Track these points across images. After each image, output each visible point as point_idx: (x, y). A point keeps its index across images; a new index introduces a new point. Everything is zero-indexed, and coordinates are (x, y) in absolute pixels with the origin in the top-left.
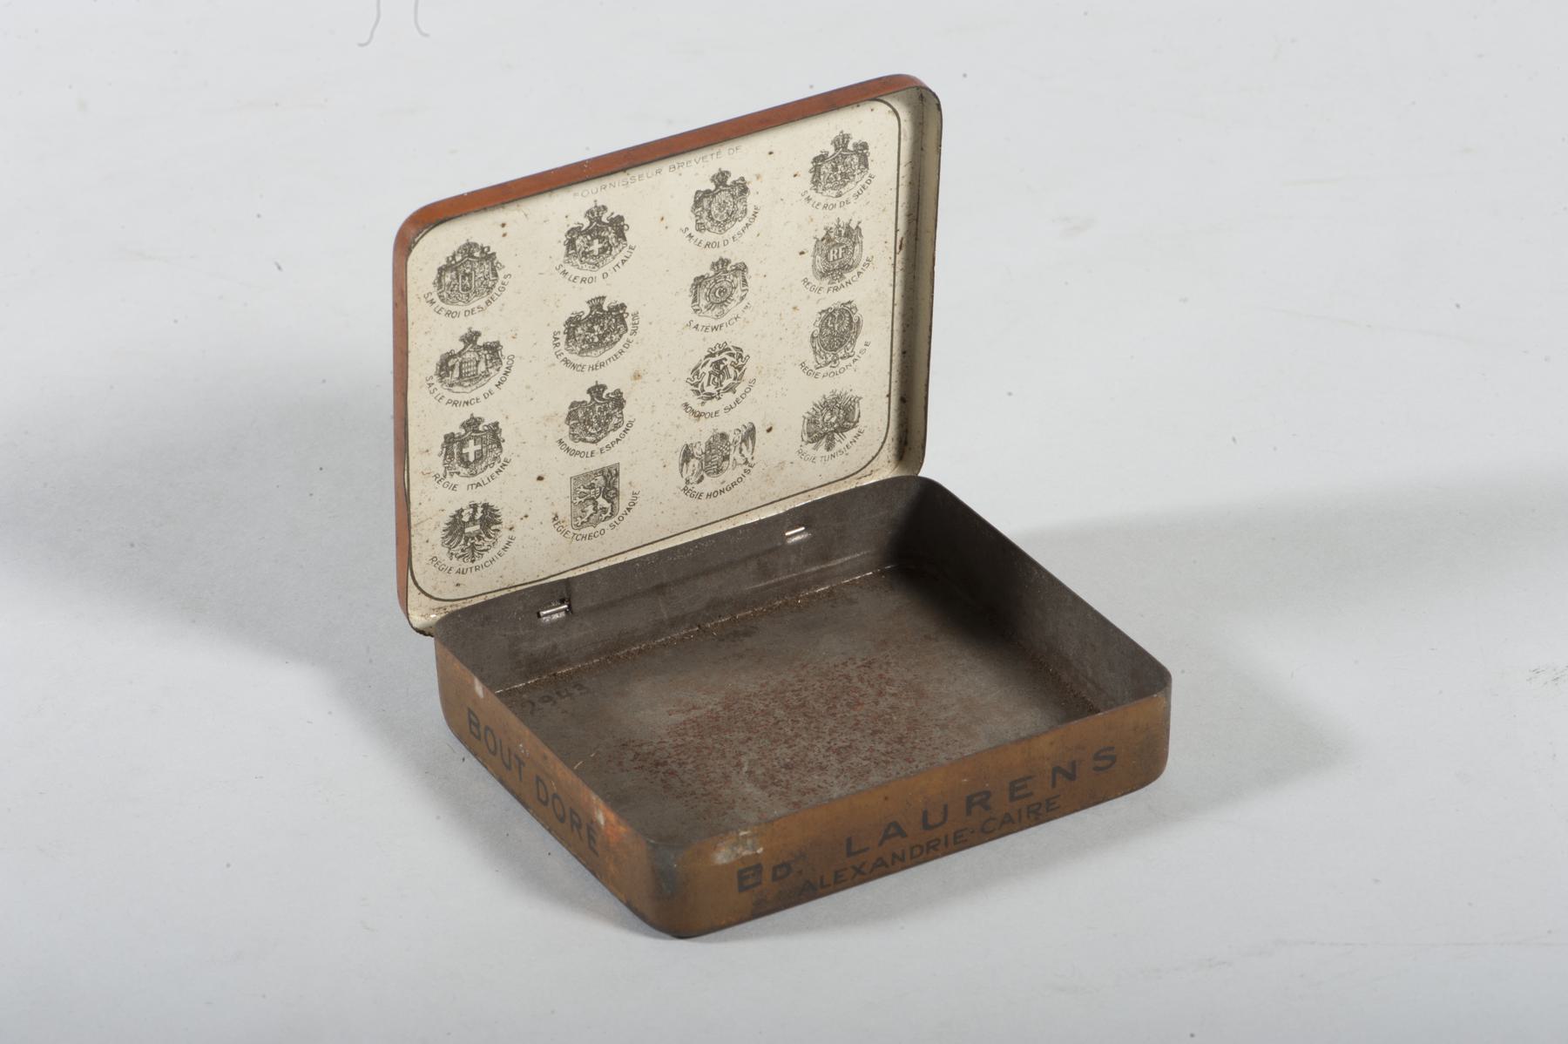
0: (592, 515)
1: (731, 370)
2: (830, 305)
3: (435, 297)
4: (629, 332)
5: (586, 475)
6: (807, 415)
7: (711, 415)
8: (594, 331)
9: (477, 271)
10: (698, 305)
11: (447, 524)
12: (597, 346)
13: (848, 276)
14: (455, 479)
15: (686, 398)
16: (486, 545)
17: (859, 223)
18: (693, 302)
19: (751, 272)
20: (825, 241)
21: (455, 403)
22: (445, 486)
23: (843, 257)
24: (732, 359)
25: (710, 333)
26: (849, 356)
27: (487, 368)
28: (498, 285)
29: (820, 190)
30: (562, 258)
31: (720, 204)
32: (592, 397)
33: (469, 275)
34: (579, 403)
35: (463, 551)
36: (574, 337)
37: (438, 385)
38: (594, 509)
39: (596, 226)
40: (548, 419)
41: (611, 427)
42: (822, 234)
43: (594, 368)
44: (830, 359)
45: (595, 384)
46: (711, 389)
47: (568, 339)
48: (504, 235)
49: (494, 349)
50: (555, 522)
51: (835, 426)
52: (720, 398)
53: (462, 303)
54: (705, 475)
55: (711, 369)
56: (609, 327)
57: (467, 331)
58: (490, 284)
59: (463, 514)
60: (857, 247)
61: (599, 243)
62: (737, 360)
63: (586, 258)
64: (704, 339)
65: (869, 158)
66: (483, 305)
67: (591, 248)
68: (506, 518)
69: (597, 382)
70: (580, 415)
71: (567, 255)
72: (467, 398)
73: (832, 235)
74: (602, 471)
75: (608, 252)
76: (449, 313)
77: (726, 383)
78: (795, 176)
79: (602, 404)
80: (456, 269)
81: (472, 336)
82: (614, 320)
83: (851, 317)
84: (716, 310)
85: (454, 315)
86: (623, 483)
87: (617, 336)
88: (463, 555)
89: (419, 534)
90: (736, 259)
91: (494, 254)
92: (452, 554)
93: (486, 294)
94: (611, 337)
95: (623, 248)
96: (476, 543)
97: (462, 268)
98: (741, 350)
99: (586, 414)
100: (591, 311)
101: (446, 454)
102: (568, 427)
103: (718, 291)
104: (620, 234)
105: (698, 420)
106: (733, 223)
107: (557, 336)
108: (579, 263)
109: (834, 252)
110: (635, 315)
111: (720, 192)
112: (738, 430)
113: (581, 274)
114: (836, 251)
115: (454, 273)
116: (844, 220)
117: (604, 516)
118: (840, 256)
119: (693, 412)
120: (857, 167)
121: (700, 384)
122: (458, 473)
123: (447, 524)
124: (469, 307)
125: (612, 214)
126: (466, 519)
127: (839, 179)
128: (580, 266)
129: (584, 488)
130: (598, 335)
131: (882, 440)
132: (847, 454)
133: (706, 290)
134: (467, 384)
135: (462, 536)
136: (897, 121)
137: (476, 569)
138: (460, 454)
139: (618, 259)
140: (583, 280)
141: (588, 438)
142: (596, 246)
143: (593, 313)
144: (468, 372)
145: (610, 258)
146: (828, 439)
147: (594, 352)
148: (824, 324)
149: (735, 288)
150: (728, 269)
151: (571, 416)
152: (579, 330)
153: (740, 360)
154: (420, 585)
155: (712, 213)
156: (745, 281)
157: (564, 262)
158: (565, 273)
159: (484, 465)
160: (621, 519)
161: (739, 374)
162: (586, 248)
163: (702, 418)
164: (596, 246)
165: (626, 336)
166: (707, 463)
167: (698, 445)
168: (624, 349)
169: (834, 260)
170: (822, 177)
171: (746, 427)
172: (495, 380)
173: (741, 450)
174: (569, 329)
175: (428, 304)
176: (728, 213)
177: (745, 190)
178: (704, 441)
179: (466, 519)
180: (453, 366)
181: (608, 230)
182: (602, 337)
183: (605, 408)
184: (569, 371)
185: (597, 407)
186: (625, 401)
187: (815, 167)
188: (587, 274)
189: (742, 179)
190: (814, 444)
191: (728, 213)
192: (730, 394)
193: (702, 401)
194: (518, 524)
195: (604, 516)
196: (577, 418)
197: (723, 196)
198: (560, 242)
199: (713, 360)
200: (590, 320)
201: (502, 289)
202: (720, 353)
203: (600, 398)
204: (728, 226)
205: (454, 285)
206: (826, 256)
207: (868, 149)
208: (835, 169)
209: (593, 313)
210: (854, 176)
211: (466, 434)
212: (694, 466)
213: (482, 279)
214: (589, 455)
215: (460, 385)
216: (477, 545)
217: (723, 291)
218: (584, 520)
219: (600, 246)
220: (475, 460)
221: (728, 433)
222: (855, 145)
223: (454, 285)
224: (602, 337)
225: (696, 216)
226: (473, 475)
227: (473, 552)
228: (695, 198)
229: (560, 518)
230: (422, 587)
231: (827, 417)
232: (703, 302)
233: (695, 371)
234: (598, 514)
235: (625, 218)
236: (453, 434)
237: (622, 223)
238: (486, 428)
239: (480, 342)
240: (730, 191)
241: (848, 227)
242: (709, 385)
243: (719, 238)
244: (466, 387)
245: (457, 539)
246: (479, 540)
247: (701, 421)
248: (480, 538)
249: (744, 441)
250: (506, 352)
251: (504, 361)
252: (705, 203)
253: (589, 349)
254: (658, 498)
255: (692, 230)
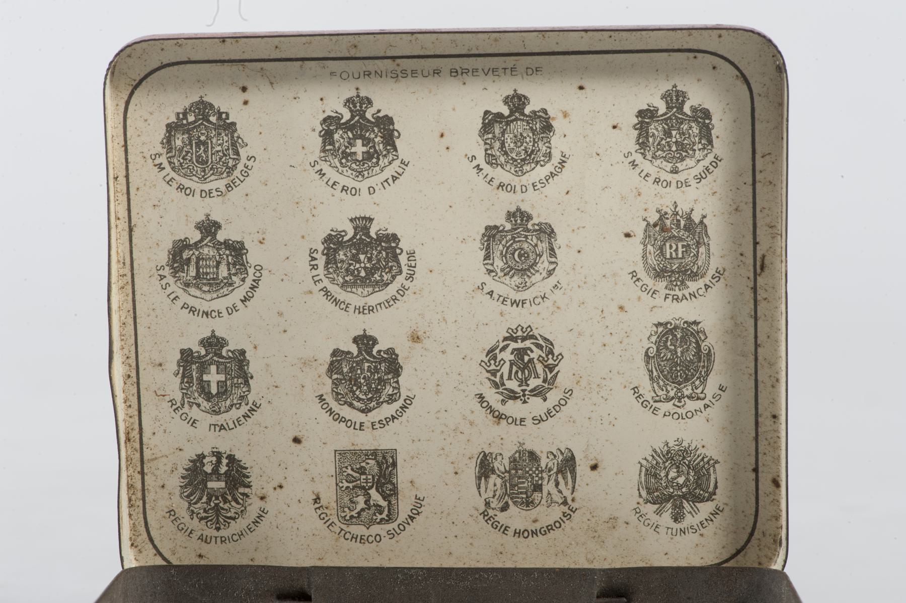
0: (363, 510)
1: (540, 368)
2: (669, 319)
3: (163, 160)
4: (404, 274)
5: (354, 453)
6: (644, 463)
7: (514, 421)
8: (359, 261)
9: (214, 140)
10: (492, 265)
11: (186, 470)
12: (364, 282)
13: (693, 286)
14: (195, 413)
15: (480, 387)
16: (233, 511)
17: (704, 217)
18: (485, 260)
19: (561, 240)
20: (658, 228)
21: (192, 310)
22: (183, 417)
23: (683, 257)
24: (540, 352)
25: (508, 308)
26: (698, 399)
27: (230, 274)
28: (240, 167)
29: (649, 157)
30: (317, 154)
31: (515, 136)
32: (359, 349)
33: (204, 143)
34: (343, 352)
35: (205, 511)
36: (336, 263)
37: (171, 280)
38: (366, 502)
39: (358, 121)
40: (305, 363)
41: (384, 397)
42: (654, 218)
43: (361, 310)
44: (672, 394)
45: (362, 333)
46: (513, 385)
47: (327, 263)
48: (246, 103)
49: (237, 250)
50: (317, 505)
51: (684, 490)
52: (525, 402)
53: (196, 179)
54: (510, 502)
55: (512, 357)
56: (379, 261)
57: (204, 218)
58: (231, 163)
59: (205, 461)
60: (702, 249)
61: (363, 145)
62: (547, 356)
63: (348, 161)
64: (501, 314)
65: (713, 132)
66: (223, 189)
67: (353, 150)
68: (257, 482)
69: (365, 330)
70: (345, 370)
71: (324, 150)
72: (205, 306)
73: (668, 222)
74: (375, 453)
75: (374, 160)
76: (181, 188)
77: (533, 383)
78: (614, 127)
79: (372, 362)
80: (188, 131)
81: (211, 227)
82: (384, 253)
83: (698, 347)
84: (515, 278)
85: (188, 191)
86: (403, 476)
87: (389, 275)
88: (206, 518)
89: (153, 473)
90: (539, 216)
91: (234, 124)
92: (193, 511)
93: (225, 175)
94: (381, 276)
95: (393, 160)
96: (221, 505)
97: (195, 133)
98: (552, 344)
99: (352, 369)
100: (355, 234)
101: (183, 377)
102: (330, 381)
103: (517, 253)
104: (390, 139)
105: (498, 423)
106: (533, 165)
107: (314, 255)
108: (338, 165)
109: (671, 247)
110: (411, 254)
111: (514, 120)
112: (552, 453)
113: (344, 181)
114: (674, 247)
115: (186, 136)
116: (684, 207)
117: (380, 517)
118: (680, 255)
119: (492, 411)
120: (697, 139)
121: (499, 374)
122: (199, 405)
123: (186, 470)
124: (206, 187)
125: (379, 111)
126: (208, 469)
127: (674, 148)
128: (341, 169)
129: (352, 469)
130: (365, 268)
131: (749, 530)
132: (702, 535)
133: (501, 247)
134: (206, 288)
135: (203, 491)
136: (748, 93)
137: (222, 541)
138: (200, 379)
139: (388, 173)
140: (344, 189)
141: (356, 403)
142: (359, 148)
143: (358, 237)
144: (207, 274)
145: (377, 168)
146: (675, 507)
147: (360, 290)
148: (661, 342)
149: (541, 256)
150: (530, 226)
151: (333, 368)
152: (341, 256)
153: (550, 356)
154: (156, 543)
155: (507, 145)
156: (552, 249)
157: (320, 158)
158: (321, 173)
159: (228, 402)
160: (402, 527)
161: (549, 376)
162: (347, 147)
163: (504, 422)
164: (359, 148)
165: (400, 279)
166: (513, 486)
167: (499, 458)
168: (399, 297)
169: (671, 258)
170: (651, 140)
171: (562, 453)
172: (240, 293)
173: (557, 484)
174: (328, 249)
175: (156, 169)
176: (526, 152)
177: (548, 127)
178: (507, 454)
179: (208, 469)
180: (189, 259)
181: (374, 131)
182: (370, 272)
183: (377, 370)
184: (330, 306)
185: (367, 365)
186: (401, 368)
187: (641, 123)
188: (350, 183)
189: (545, 111)
190: (656, 506)
191: (526, 152)
192: (539, 400)
193: (501, 398)
194: (272, 495)
195: (380, 517)
196: (342, 373)
197: (519, 127)
198: (314, 130)
199: (513, 345)
200: (354, 244)
201: (246, 173)
202: (524, 339)
203: (370, 354)
204: (527, 168)
205: (187, 152)
206: (661, 248)
207: (711, 119)
208: (668, 134)
209: (358, 237)
210: (695, 150)
211: (206, 355)
212: (495, 485)
213: (221, 154)
214: (358, 426)
215: (198, 287)
216: (223, 509)
217: (524, 255)
218: (354, 513)
219: (365, 149)
220: (218, 393)
221: (538, 453)
222: (694, 109)
223: (187, 152)
224: (370, 272)
225: (486, 144)
226: (217, 413)
227: (218, 516)
228: (484, 119)
229: (323, 502)
230: (159, 546)
231: (672, 474)
232: (499, 264)
233: (491, 353)
234: (371, 512)
235: (395, 120)
236: (190, 350)
237: (391, 127)
238: (230, 354)
239: (221, 236)
240: (528, 123)
241: (689, 218)
242: (510, 378)
243: (516, 181)
244: (205, 292)
245: (198, 494)
246: (225, 502)
247: (501, 426)
248: (225, 501)
249: (560, 471)
250: (253, 256)
251: (251, 271)
252: (497, 130)
253: (354, 284)
254: (449, 514)
255: (481, 160)
